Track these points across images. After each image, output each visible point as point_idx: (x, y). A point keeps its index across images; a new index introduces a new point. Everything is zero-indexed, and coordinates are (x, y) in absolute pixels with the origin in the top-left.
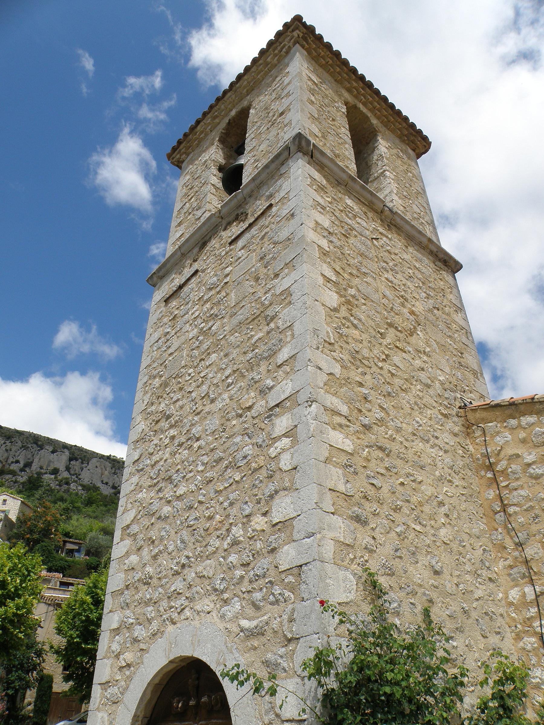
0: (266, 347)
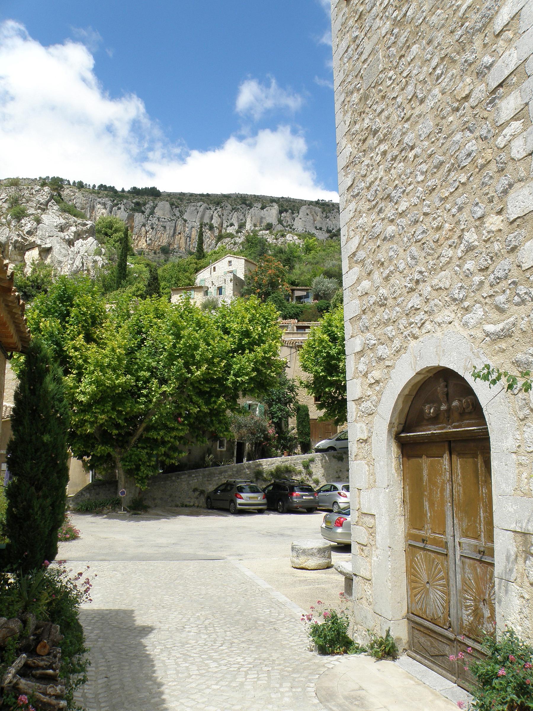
0: (478, 16)
